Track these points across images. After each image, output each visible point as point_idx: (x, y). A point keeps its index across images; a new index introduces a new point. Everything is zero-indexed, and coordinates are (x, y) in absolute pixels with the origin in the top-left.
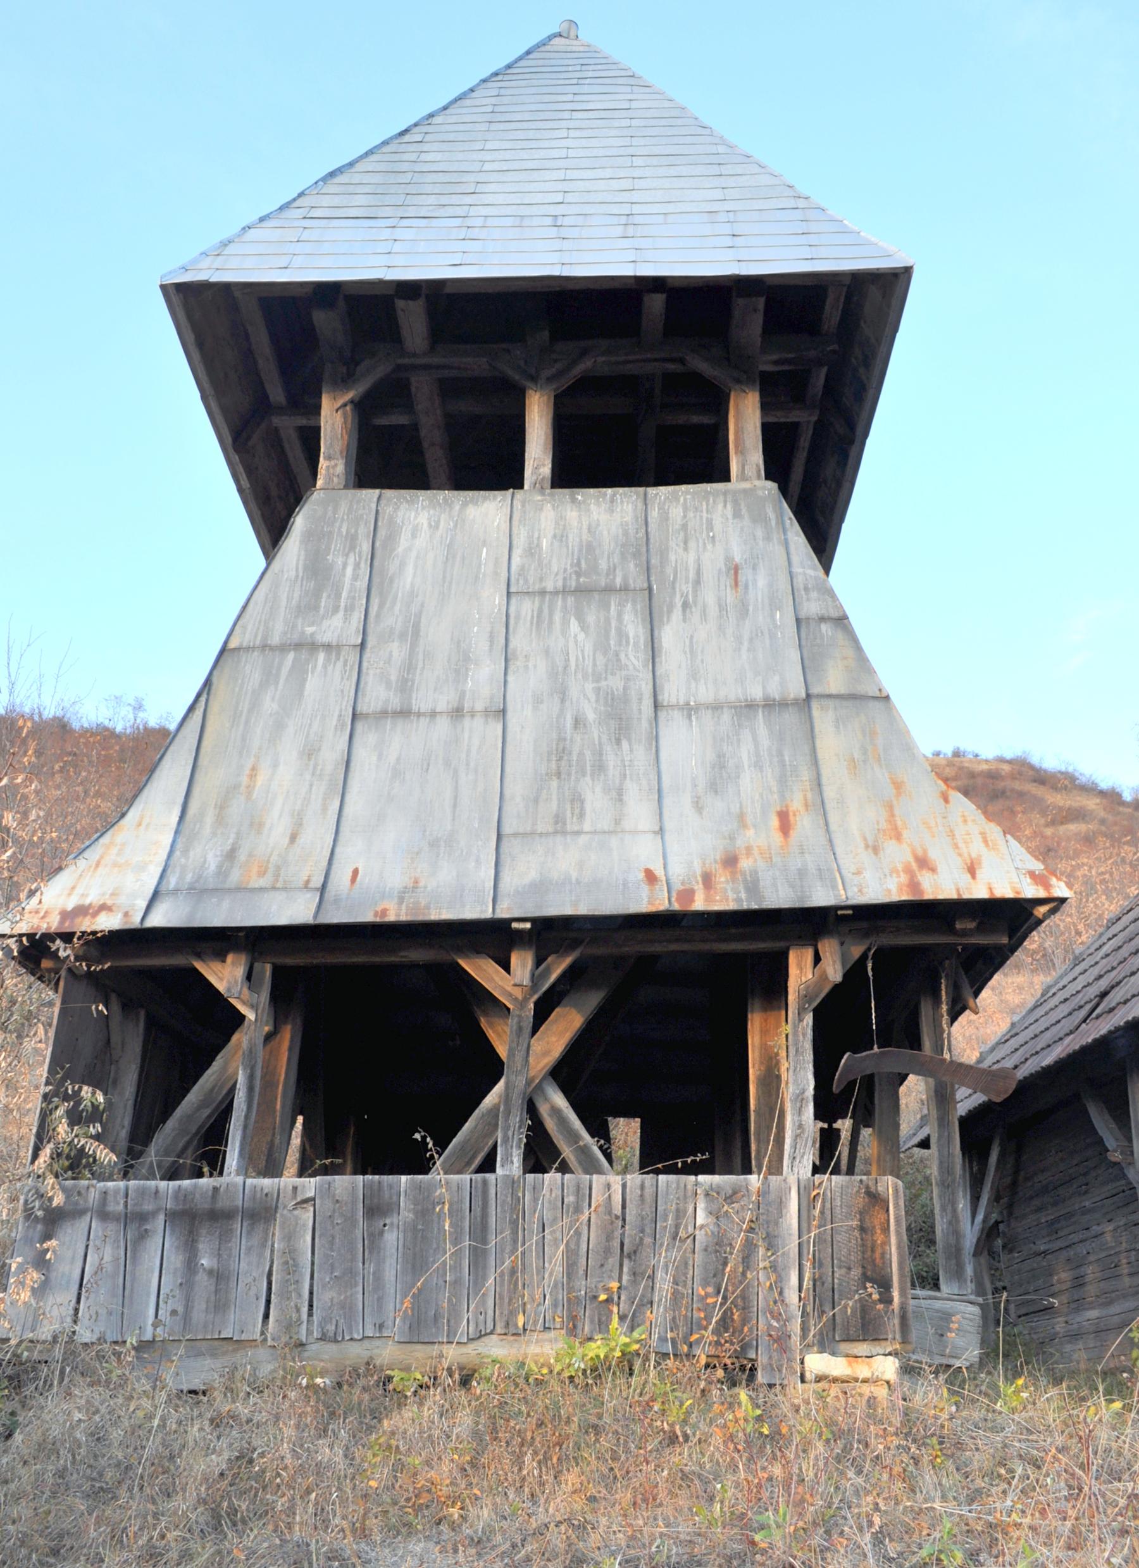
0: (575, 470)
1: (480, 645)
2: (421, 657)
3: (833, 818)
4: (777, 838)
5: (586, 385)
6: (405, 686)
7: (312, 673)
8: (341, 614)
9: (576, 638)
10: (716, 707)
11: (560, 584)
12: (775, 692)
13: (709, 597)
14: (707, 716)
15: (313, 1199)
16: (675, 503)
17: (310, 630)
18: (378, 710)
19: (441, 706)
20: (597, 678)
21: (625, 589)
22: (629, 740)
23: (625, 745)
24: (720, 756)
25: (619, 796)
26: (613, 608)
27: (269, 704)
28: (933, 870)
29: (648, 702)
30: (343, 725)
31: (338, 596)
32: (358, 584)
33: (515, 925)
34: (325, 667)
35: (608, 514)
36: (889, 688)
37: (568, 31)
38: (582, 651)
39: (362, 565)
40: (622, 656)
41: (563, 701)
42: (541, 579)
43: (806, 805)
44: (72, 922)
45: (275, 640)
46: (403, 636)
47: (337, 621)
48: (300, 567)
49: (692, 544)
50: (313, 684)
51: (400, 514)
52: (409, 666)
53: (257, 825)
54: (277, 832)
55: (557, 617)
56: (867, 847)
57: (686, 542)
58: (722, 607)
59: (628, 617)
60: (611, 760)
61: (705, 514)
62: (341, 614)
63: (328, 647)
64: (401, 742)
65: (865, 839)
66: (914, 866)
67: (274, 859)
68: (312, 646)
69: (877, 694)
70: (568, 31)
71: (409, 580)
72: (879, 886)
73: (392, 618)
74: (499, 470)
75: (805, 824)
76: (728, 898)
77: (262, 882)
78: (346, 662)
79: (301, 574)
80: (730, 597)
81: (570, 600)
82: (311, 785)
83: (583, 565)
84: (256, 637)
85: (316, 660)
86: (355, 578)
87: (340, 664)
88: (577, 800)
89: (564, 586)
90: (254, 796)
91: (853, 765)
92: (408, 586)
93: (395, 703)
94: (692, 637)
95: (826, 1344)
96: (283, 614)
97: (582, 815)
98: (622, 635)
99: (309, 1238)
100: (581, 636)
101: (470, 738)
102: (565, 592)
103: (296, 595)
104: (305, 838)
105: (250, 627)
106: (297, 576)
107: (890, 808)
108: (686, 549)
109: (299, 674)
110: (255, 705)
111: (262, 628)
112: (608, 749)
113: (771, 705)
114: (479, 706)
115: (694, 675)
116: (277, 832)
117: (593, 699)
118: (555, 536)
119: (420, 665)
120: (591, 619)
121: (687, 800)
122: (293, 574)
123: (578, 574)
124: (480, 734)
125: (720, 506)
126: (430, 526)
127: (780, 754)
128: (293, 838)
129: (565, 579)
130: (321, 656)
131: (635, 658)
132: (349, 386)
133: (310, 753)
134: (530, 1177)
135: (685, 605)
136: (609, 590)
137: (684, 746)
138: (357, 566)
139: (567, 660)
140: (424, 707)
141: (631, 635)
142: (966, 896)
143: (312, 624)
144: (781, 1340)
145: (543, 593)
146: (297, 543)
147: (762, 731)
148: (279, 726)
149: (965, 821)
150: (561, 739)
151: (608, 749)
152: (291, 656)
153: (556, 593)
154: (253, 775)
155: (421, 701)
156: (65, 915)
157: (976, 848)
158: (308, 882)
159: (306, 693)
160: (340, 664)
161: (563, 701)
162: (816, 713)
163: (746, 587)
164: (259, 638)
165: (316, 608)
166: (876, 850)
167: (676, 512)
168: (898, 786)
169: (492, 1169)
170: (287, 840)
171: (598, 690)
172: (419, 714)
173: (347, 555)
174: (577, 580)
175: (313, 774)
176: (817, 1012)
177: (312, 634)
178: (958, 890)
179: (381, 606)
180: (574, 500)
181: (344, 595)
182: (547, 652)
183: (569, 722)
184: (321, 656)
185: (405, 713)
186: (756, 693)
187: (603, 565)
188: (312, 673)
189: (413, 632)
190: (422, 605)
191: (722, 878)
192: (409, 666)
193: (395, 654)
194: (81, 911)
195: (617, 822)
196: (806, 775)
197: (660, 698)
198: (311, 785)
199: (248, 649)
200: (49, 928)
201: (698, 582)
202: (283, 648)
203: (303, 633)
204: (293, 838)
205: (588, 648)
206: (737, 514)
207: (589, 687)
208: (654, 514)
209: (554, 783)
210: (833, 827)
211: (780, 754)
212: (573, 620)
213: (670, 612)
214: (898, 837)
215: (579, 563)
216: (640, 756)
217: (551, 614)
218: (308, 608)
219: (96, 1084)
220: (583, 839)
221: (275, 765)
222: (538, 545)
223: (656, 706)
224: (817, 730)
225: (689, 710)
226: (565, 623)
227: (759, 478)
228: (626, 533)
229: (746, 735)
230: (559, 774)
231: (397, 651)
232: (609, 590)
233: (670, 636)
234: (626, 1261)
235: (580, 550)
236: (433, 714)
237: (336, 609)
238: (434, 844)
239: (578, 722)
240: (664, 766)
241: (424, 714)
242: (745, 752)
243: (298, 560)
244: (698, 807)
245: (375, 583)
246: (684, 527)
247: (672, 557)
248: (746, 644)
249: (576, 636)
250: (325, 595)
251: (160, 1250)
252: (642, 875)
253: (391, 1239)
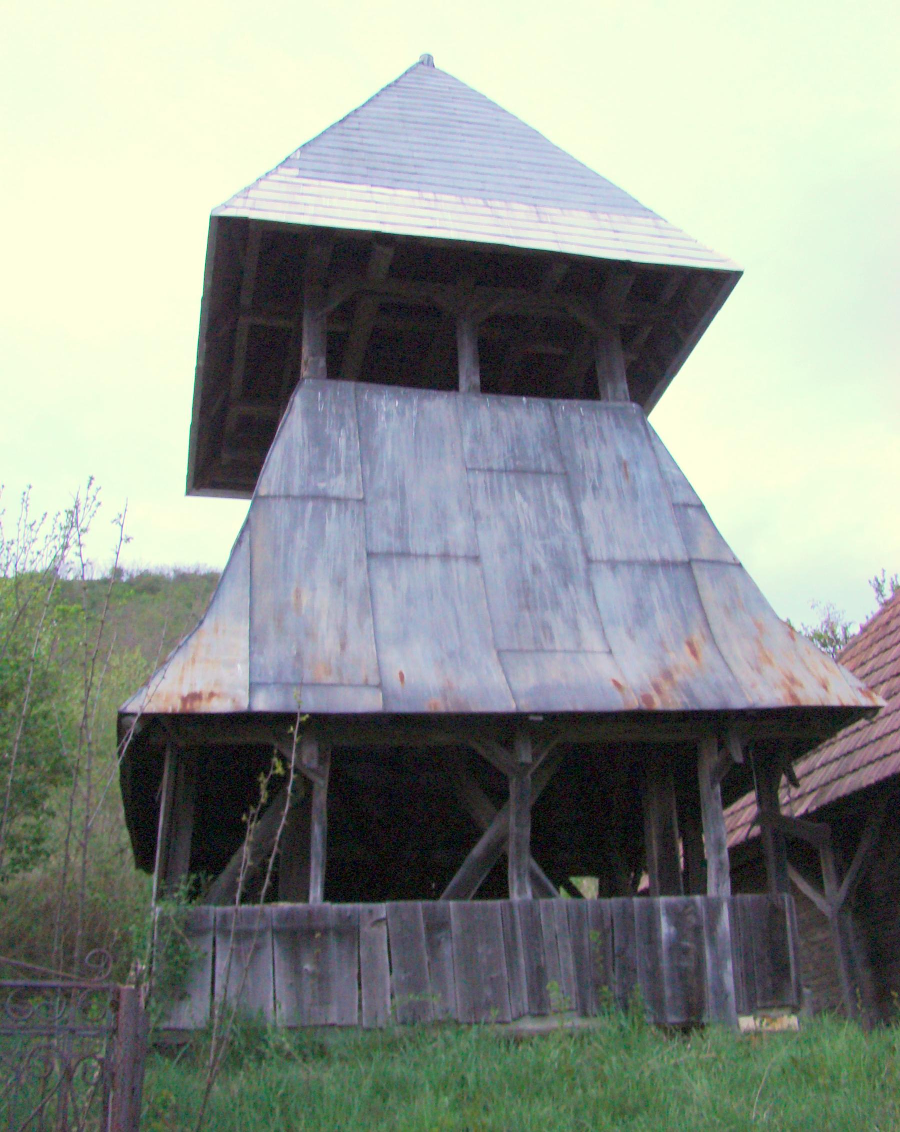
0: (493, 384)
1: (453, 507)
2: (410, 513)
3: (724, 647)
4: (691, 659)
5: (493, 320)
6: (401, 533)
7: (329, 519)
8: (342, 475)
9: (520, 505)
10: (630, 563)
11: (502, 465)
12: (667, 556)
13: (609, 482)
14: (624, 570)
15: (385, 919)
16: (574, 414)
17: (322, 486)
18: (385, 550)
19: (432, 550)
20: (543, 538)
21: (549, 472)
22: (574, 584)
23: (571, 588)
24: (639, 599)
25: (575, 626)
26: (544, 486)
27: (301, 542)
28: (801, 685)
29: (581, 559)
30: (360, 561)
31: (338, 461)
32: (352, 453)
33: (532, 718)
34: (338, 514)
35: (526, 417)
36: (741, 558)
37: (427, 62)
38: (528, 516)
39: (352, 438)
40: (557, 521)
41: (521, 552)
42: (488, 460)
43: (703, 636)
44: (191, 705)
45: (296, 491)
46: (393, 496)
47: (341, 480)
48: (306, 436)
49: (591, 444)
50: (331, 527)
51: (375, 401)
52: (403, 518)
53: (310, 634)
54: (328, 642)
55: (505, 489)
56: (752, 669)
57: (586, 442)
58: (620, 492)
59: (555, 493)
60: (564, 600)
61: (596, 422)
62: (342, 475)
63: (338, 499)
64: (410, 576)
65: (749, 663)
66: (788, 682)
67: (333, 661)
68: (323, 498)
69: (733, 561)
70: (427, 62)
71: (390, 453)
72: (769, 696)
73: (383, 481)
74: (445, 381)
75: (706, 651)
76: (671, 700)
77: (330, 679)
78: (353, 512)
79: (307, 442)
80: (625, 486)
81: (512, 478)
82: (346, 607)
83: (516, 451)
84: (280, 488)
85: (331, 510)
86: (348, 447)
87: (349, 513)
88: (546, 627)
89: (506, 467)
90: (303, 611)
91: (728, 611)
92: (390, 457)
93: (397, 546)
94: (603, 512)
95: (750, 1009)
96: (298, 471)
97: (552, 639)
98: (555, 508)
99: (385, 948)
100: (525, 505)
101: (458, 576)
102: (506, 471)
103: (306, 457)
104: (352, 647)
105: (274, 480)
106: (304, 443)
107: (758, 641)
108: (587, 447)
109: (319, 518)
110: (290, 541)
111: (283, 482)
112: (560, 591)
113: (667, 564)
114: (461, 553)
115: (610, 539)
116: (328, 642)
117: (542, 552)
118: (492, 429)
119: (411, 518)
120: (530, 492)
121: (622, 631)
122: (300, 441)
123: (515, 459)
124: (461, 571)
125: (605, 419)
126: (398, 413)
127: (678, 599)
128: (343, 646)
129: (505, 461)
130: (334, 507)
131: (566, 524)
132: (307, 320)
133: (339, 581)
134: (542, 901)
135: (594, 488)
136: (538, 472)
137: (611, 590)
138: (348, 439)
139: (518, 521)
140: (420, 550)
141: (561, 507)
142: (826, 704)
143: (323, 481)
144: (721, 1005)
145: (491, 470)
146: (300, 418)
147: (664, 584)
148: (310, 561)
149: (809, 653)
150: (525, 581)
151: (560, 591)
152: (310, 505)
153: (500, 471)
154: (298, 593)
155: (417, 545)
156: (184, 700)
157: (822, 672)
158: (367, 680)
159: (327, 534)
160: (349, 513)
161: (521, 552)
162: (696, 572)
163: (634, 477)
164: (283, 489)
165: (323, 469)
166: (759, 670)
167: (575, 419)
168: (759, 626)
169: (503, 893)
170: (338, 648)
171: (545, 546)
172: (416, 556)
173: (340, 430)
174: (515, 464)
175: (345, 598)
176: (722, 783)
177: (324, 489)
178: (839, 699)
179: (372, 470)
180: (500, 403)
181: (343, 460)
182: (502, 515)
183: (528, 569)
184: (334, 507)
185: (405, 554)
186: (655, 555)
187: (530, 452)
188: (329, 519)
189: (401, 493)
190: (404, 472)
191: (666, 687)
192: (403, 518)
193: (390, 509)
194: (195, 696)
195: (579, 644)
196: (698, 616)
197: (589, 555)
198: (346, 607)
199: (274, 497)
200: (174, 710)
201: (600, 471)
202: (304, 498)
203: (316, 487)
204: (343, 646)
205: (532, 514)
206: (618, 425)
207: (539, 543)
208: (560, 420)
209: (526, 614)
210: (725, 653)
211: (678, 599)
212: (516, 493)
213: (584, 491)
214: (770, 662)
215: (513, 450)
216: (583, 595)
217: (500, 487)
218: (316, 468)
219: (314, 934)
220: (559, 656)
221: (314, 589)
222: (481, 434)
223: (589, 561)
224: (699, 584)
225: (613, 564)
226: (512, 496)
227: (626, 399)
228: (543, 431)
229: (653, 585)
230: (528, 608)
231: (391, 506)
232: (538, 472)
233: (587, 507)
234: (617, 959)
235: (513, 440)
236: (427, 556)
237: (338, 471)
238: (451, 655)
239: (535, 569)
240: (601, 605)
241: (420, 556)
242: (655, 596)
243: (303, 431)
244: (632, 637)
245: (368, 453)
246: (583, 430)
247: (579, 452)
248: (641, 521)
249: (521, 505)
250: (328, 459)
251: (273, 956)
252: (611, 684)
253: (448, 950)
